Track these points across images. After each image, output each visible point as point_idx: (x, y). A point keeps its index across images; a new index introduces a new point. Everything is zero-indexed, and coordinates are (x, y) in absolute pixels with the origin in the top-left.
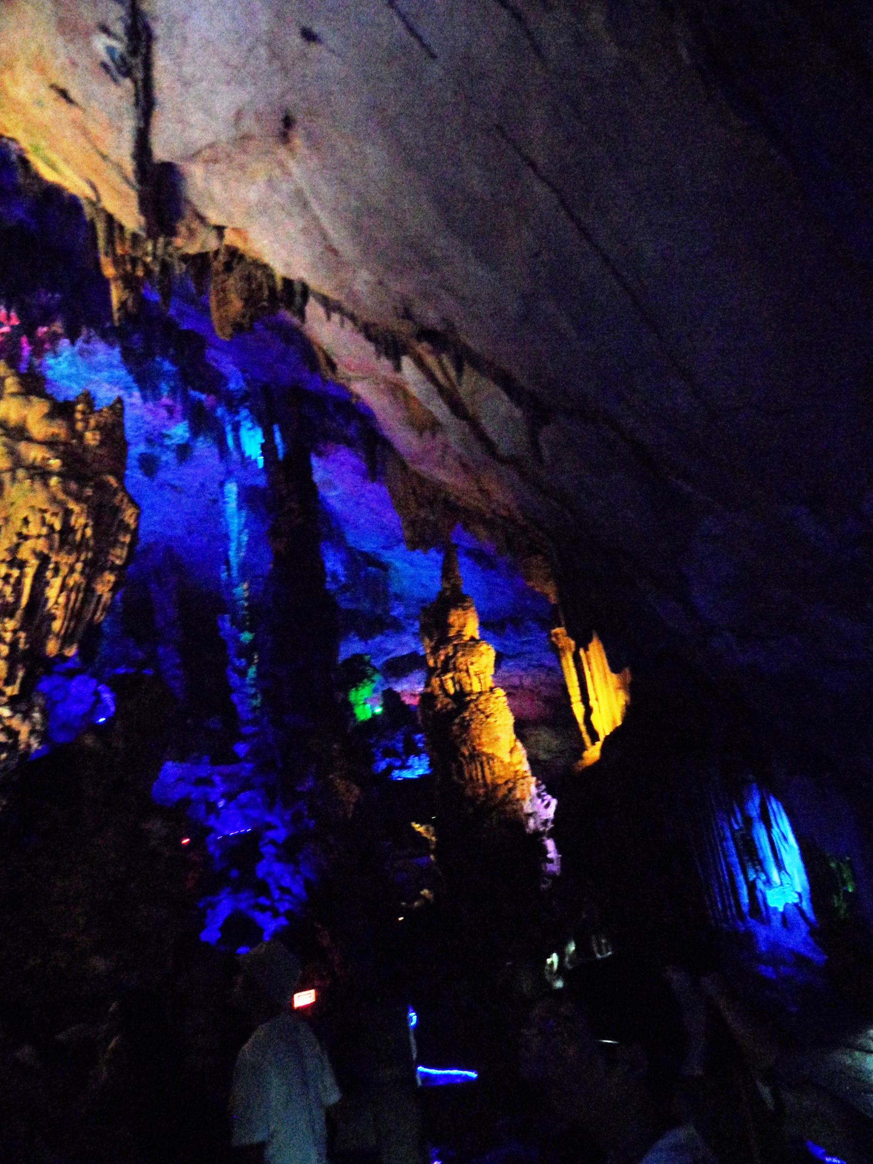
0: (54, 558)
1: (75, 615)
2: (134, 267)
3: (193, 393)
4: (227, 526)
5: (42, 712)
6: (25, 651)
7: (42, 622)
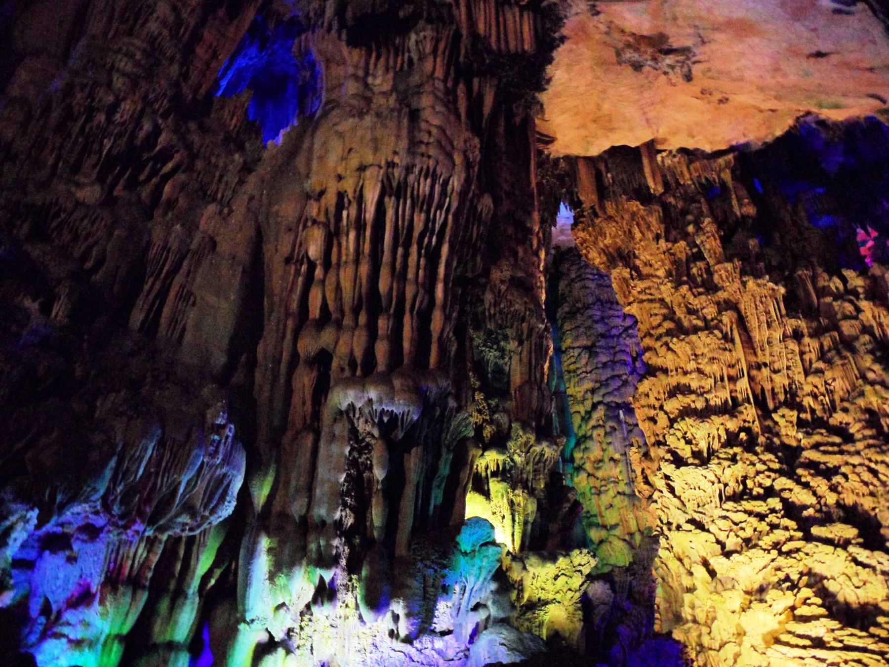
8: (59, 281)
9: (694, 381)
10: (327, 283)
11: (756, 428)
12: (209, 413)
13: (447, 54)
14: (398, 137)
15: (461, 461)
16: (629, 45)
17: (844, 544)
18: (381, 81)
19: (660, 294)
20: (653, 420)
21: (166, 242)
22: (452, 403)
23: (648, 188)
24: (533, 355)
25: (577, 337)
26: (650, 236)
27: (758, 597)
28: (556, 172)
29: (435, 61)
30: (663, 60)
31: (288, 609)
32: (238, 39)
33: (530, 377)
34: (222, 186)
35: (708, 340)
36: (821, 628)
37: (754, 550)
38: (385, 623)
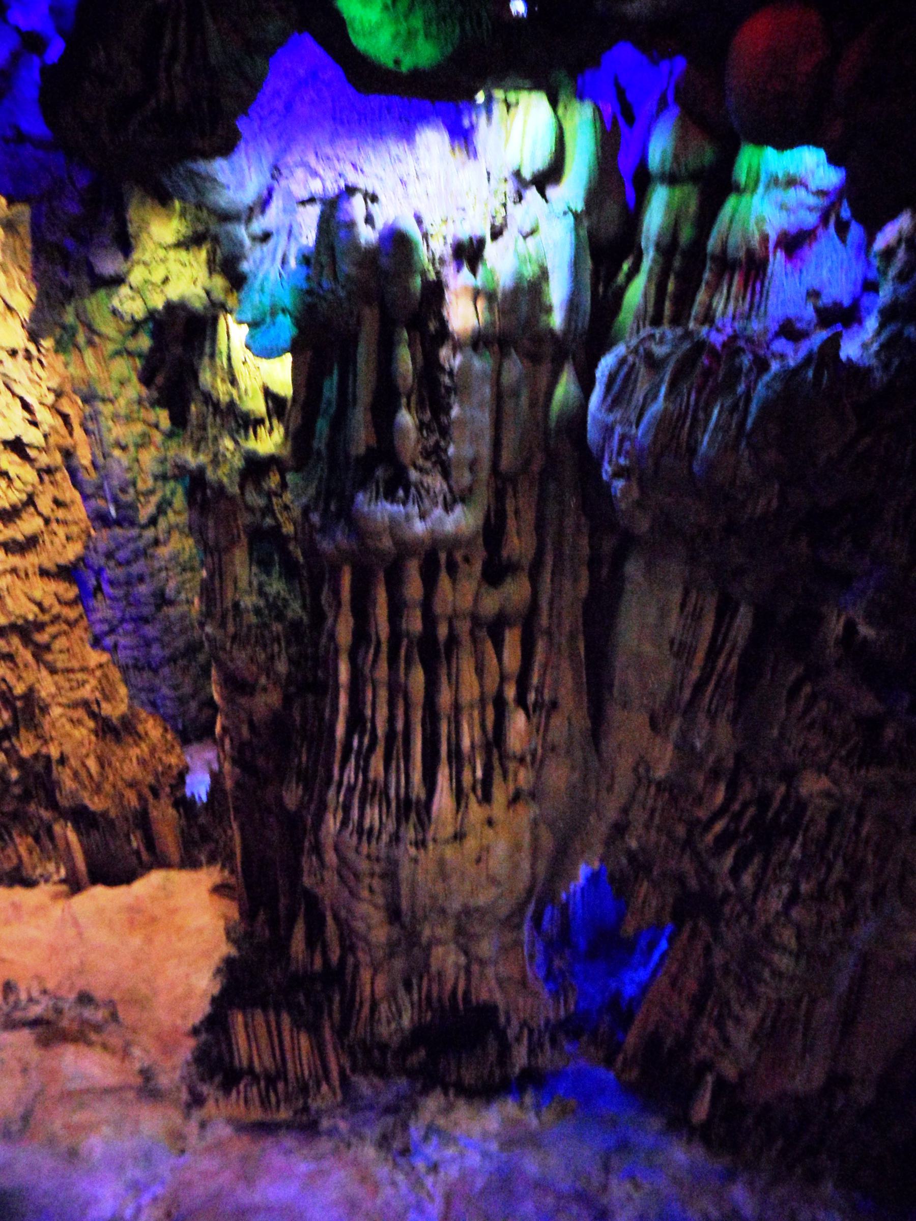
8: (838, 664)
10: (498, 679)
12: (635, 494)
14: (413, 885)
15: (300, 439)
16: (97, 1028)
18: (447, 959)
19: (56, 684)
20: (58, 503)
21: (713, 724)
22: (315, 518)
23: (77, 829)
25: (183, 617)
26: (73, 762)
28: (213, 845)
29: (373, 991)
30: (46, 1010)
31: (521, 232)
32: (644, 1008)
34: (650, 802)
38: (384, 215)
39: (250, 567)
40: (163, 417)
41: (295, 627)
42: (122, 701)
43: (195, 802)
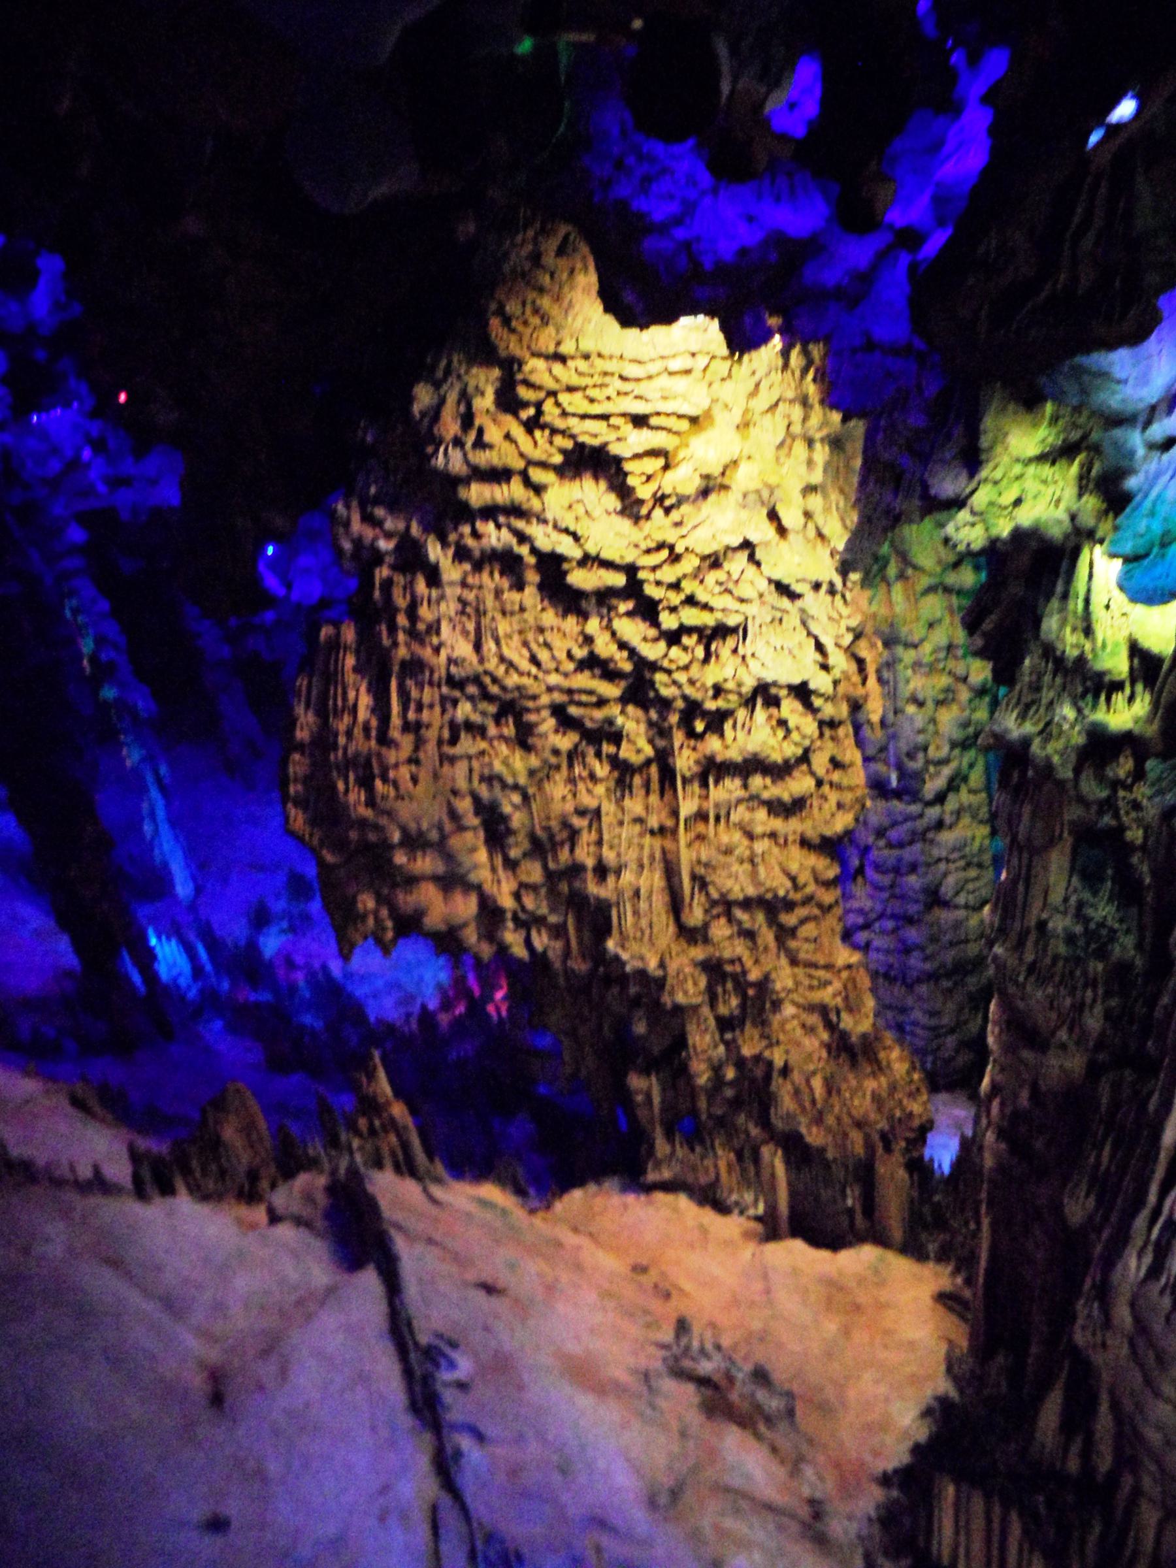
0: (373, 743)
1: (332, 677)
2: (371, 1125)
3: (266, 997)
4: (176, 838)
5: (340, 551)
6: (379, 623)
7: (369, 661)
9: (761, 820)
11: (679, 737)
13: (1128, 1553)
16: (769, 1420)
17: (587, 560)
19: (794, 976)
20: (836, 764)
23: (787, 1162)
24: (1020, 898)
25: (957, 925)
26: (796, 1076)
27: (711, 483)
33: (1030, 861)
35: (729, 883)
36: (628, 443)
37: (707, 552)
39: (1070, 877)
40: (980, 671)
41: (1122, 970)
42: (867, 1017)
43: (932, 1171)
